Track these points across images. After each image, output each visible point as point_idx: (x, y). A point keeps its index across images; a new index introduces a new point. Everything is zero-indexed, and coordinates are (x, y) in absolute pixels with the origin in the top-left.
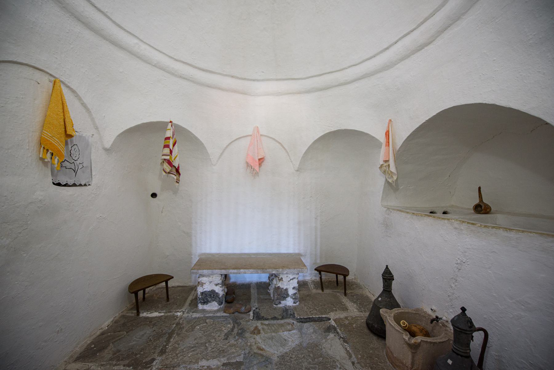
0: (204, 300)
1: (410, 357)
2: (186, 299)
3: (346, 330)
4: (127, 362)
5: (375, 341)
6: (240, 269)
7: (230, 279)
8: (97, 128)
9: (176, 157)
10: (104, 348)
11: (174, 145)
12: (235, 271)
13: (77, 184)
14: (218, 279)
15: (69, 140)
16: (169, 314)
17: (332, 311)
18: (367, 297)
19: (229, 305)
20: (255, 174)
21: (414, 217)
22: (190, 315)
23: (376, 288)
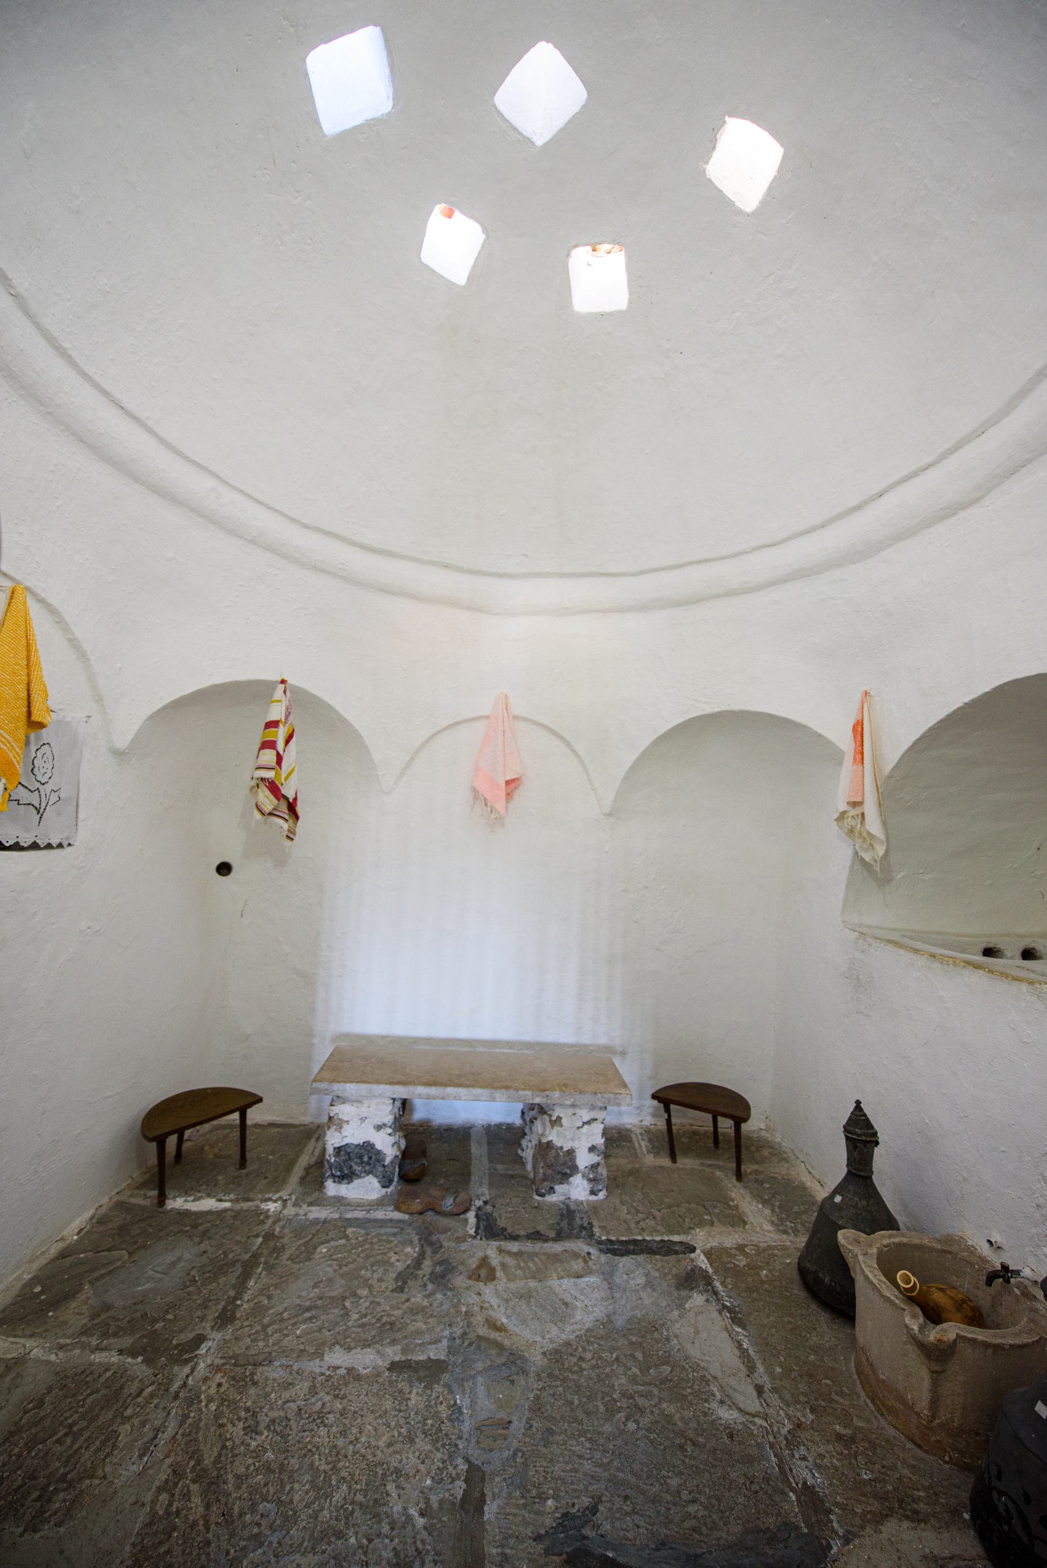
0: (341, 1171)
1: (926, 1383)
2: (292, 1163)
3: (736, 1283)
4: (127, 1341)
5: (824, 1329)
6: (445, 1085)
7: (412, 1110)
8: (99, 700)
9: (292, 771)
10: (68, 1296)
11: (287, 742)
12: (433, 1091)
13: (41, 843)
14: (386, 1114)
15: (32, 736)
16: (246, 1205)
17: (701, 1224)
18: (803, 1188)
19: (409, 1188)
20: (496, 820)
21: (936, 965)
22: (301, 1212)
23: (825, 1168)
